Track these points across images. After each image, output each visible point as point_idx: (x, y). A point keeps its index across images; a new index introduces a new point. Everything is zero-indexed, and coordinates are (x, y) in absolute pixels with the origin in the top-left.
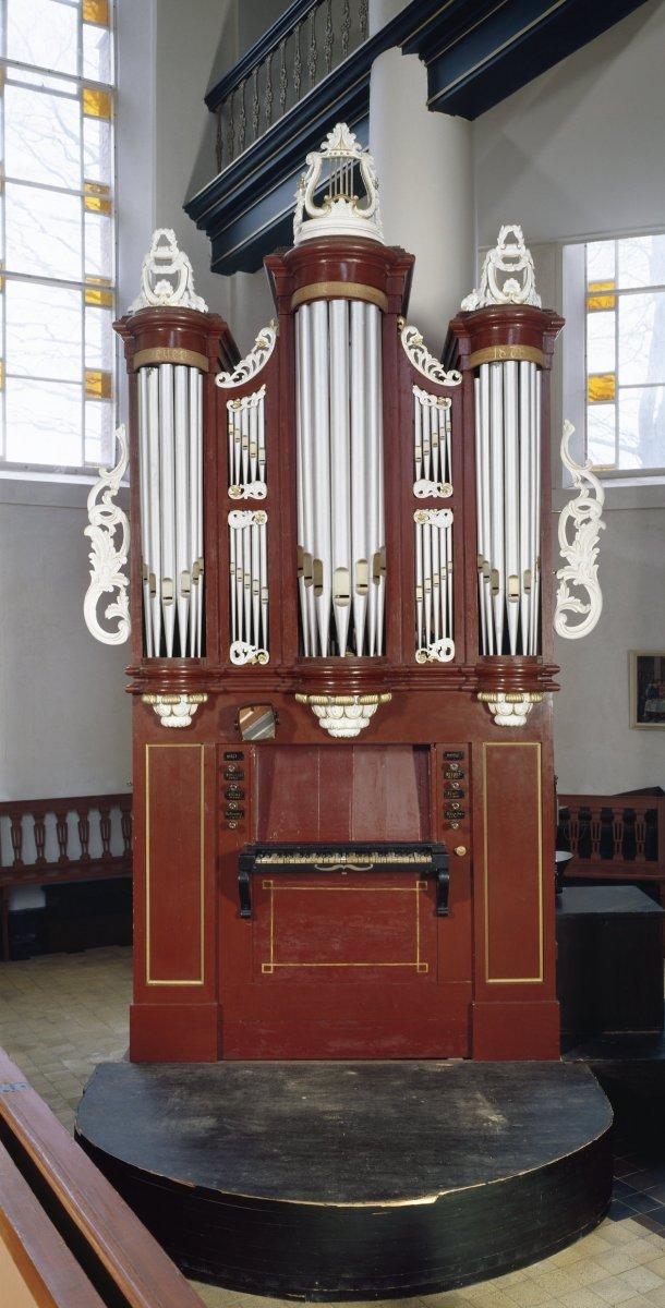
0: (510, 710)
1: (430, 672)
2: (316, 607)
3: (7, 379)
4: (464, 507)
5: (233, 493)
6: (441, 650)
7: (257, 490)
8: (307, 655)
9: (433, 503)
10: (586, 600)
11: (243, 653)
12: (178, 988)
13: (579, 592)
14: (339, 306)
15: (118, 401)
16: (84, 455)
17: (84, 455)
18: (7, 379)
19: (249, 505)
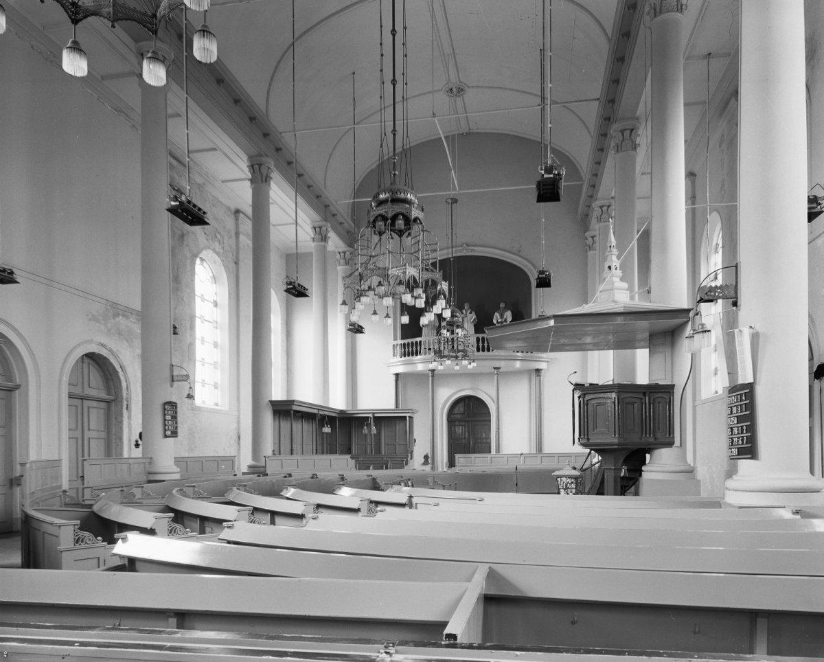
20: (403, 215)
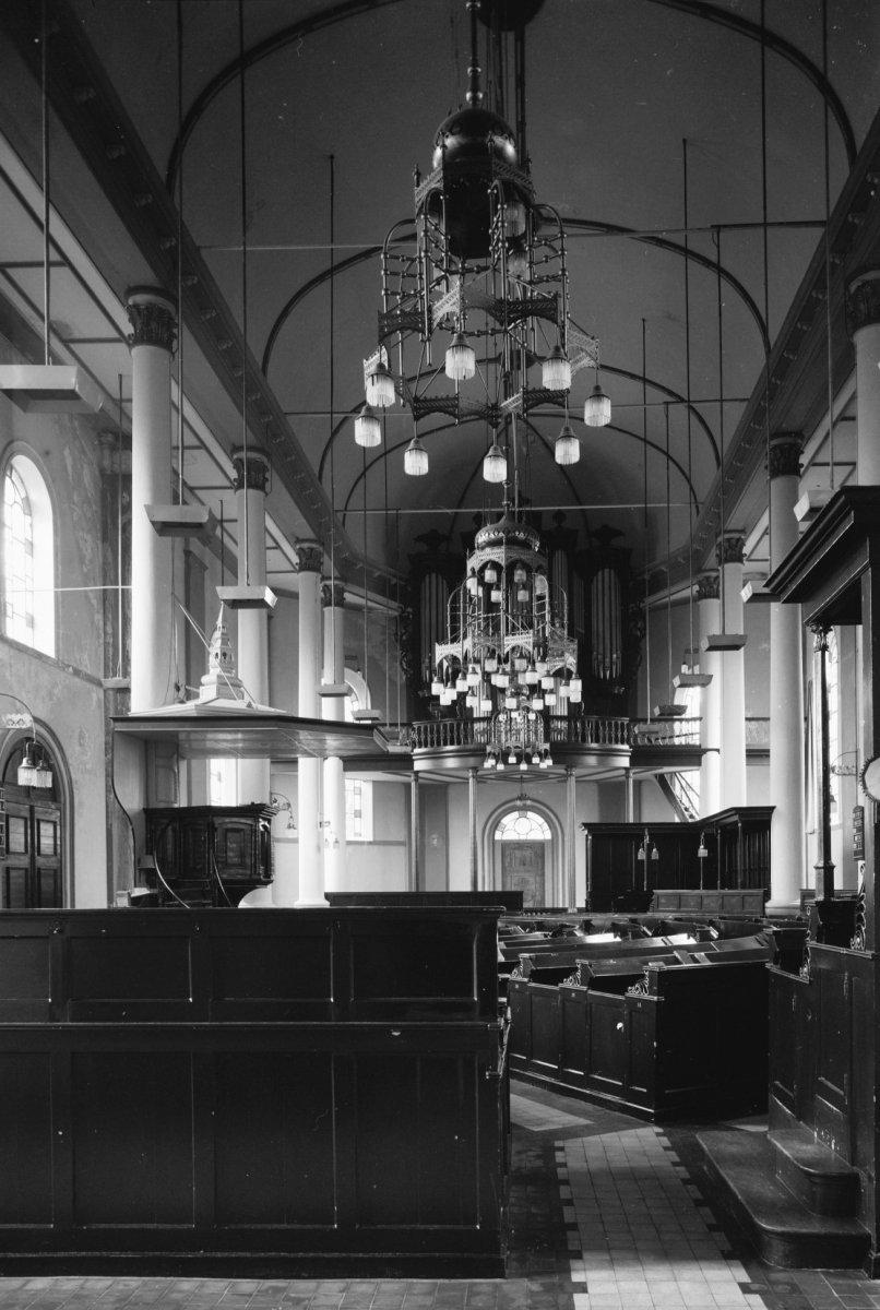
20: (521, 561)
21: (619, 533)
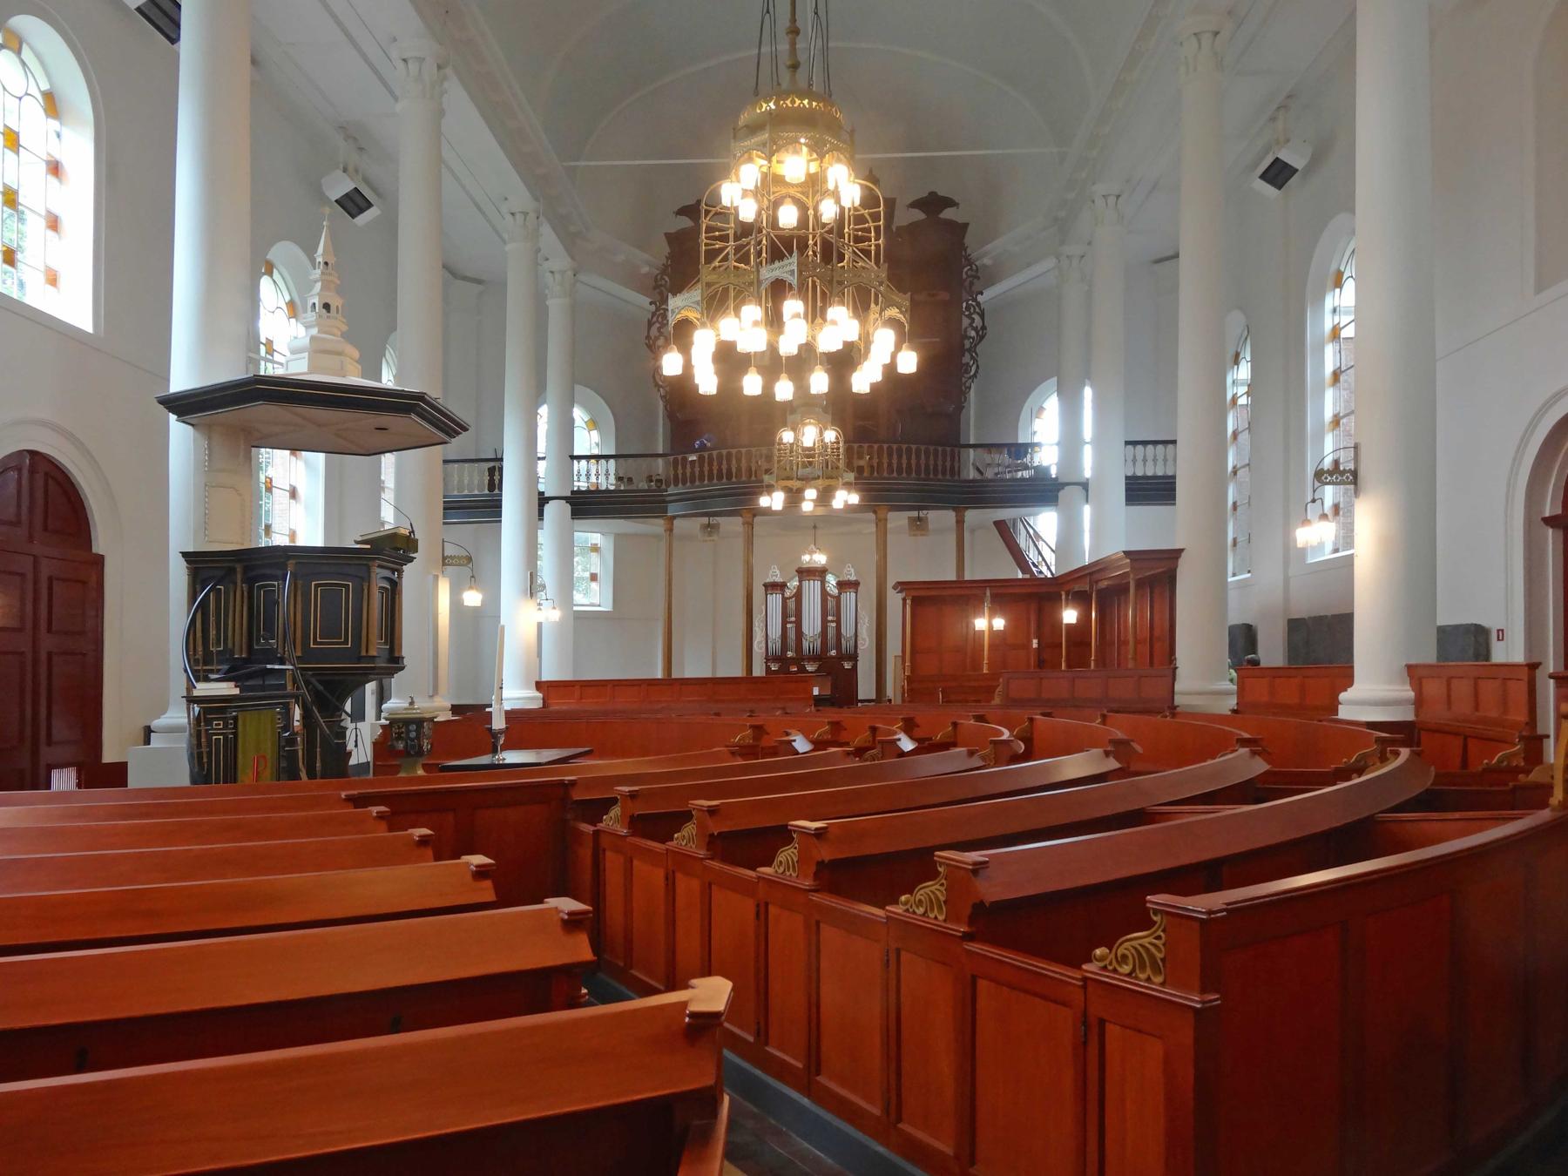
0: (847, 666)
1: (447, 414)
2: (805, 645)
3: (152, 734)
4: (838, 622)
5: (788, 620)
6: (833, 653)
7: (793, 619)
8: (1219, 1002)
9: (832, 621)
10: (865, 641)
11: (790, 654)
12: (645, 158)
13: (864, 640)
14: (812, 582)
15: (1438, 666)
16: (39, 88)
17: (39, 88)
18: (152, 734)
19: (791, 622)
21: (949, 203)
